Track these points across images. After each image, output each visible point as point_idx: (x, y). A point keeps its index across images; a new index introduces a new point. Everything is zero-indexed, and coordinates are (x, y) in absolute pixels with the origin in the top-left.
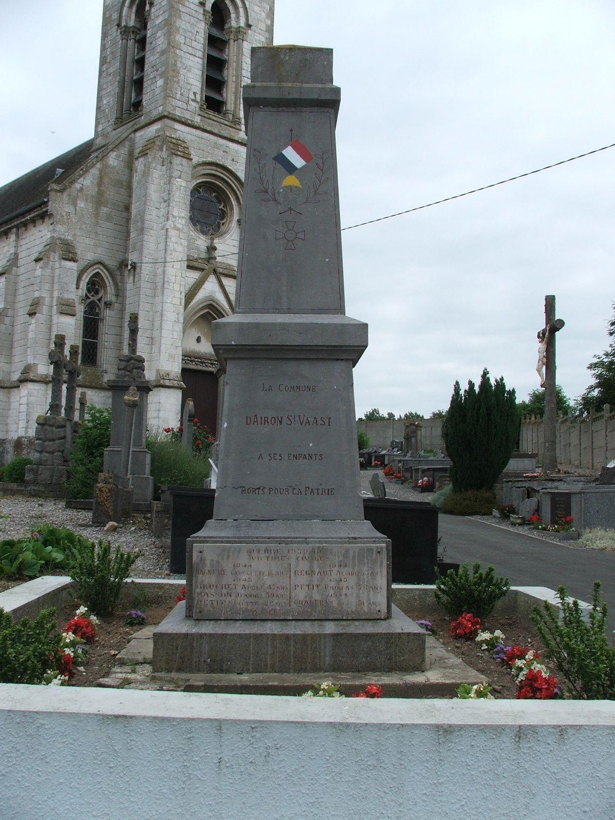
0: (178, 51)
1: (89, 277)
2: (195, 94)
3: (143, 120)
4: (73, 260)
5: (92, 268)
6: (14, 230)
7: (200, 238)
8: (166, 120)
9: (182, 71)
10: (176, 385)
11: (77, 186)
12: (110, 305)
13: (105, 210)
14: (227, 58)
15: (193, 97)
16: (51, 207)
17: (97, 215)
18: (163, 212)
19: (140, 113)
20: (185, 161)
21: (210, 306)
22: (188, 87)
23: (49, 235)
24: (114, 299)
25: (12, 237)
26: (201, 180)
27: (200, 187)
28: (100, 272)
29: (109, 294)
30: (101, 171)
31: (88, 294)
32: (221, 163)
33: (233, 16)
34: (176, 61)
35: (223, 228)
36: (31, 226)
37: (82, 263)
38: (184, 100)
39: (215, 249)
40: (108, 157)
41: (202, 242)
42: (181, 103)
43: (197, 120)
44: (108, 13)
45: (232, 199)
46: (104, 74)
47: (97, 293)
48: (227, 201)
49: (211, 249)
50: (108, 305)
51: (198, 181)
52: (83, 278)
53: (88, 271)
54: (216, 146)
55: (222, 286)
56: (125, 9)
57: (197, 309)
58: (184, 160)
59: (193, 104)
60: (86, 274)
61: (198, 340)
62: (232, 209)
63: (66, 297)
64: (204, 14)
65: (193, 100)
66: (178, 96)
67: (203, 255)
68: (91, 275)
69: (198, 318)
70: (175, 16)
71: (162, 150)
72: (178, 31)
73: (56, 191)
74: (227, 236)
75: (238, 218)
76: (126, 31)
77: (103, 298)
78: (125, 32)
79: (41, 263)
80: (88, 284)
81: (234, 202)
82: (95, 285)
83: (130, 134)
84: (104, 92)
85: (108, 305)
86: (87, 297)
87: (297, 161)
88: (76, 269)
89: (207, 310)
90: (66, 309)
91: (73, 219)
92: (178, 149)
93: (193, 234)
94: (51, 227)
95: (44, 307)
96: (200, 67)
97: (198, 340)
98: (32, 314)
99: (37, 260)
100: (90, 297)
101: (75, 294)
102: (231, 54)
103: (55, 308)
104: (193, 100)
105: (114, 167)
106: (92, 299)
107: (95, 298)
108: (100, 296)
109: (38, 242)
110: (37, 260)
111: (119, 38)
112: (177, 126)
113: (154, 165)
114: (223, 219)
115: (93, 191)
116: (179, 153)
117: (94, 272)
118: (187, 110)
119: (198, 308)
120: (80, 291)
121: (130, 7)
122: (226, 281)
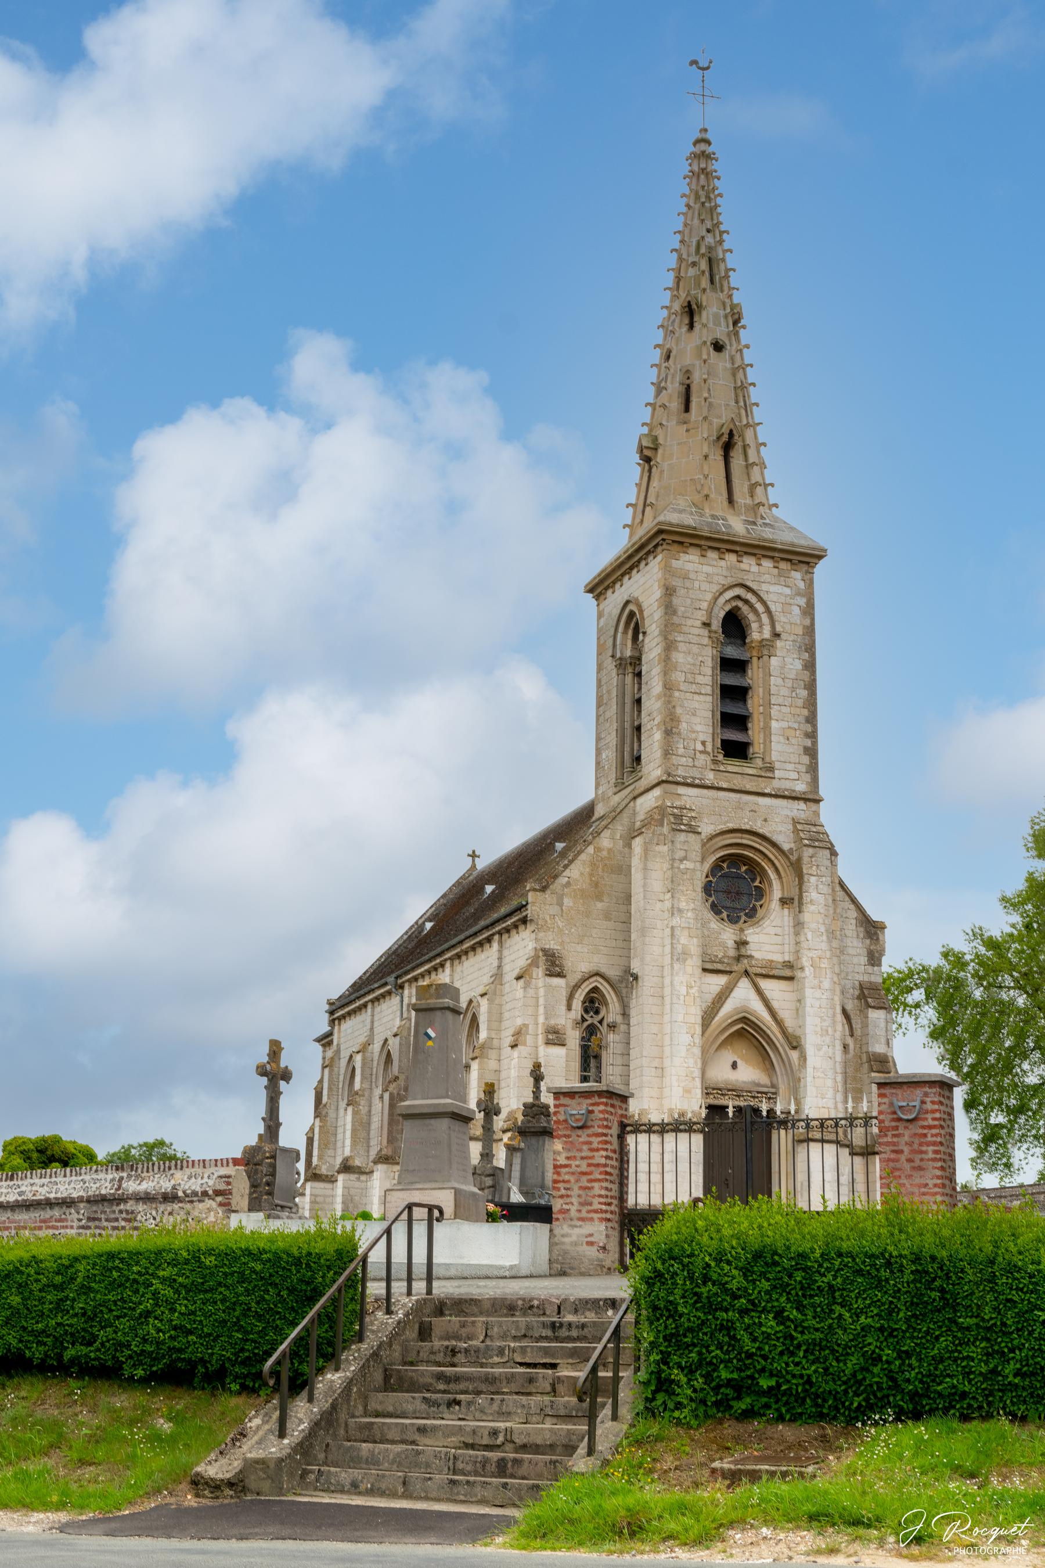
0: (677, 694)
1: (584, 993)
2: (703, 743)
3: (643, 784)
4: (560, 975)
5: (587, 982)
6: (496, 937)
8: (664, 785)
9: (684, 718)
11: (562, 880)
14: (750, 682)
16: (530, 912)
18: (668, 904)
19: (640, 774)
20: (692, 837)
21: (744, 1020)
22: (694, 736)
23: (531, 945)
24: (619, 1019)
25: (495, 945)
27: (723, 862)
29: (612, 1012)
32: (747, 827)
33: (754, 626)
35: (760, 912)
36: (514, 932)
37: (574, 978)
39: (745, 943)
41: (728, 935)
43: (710, 777)
44: (602, 638)
45: (769, 872)
46: (601, 719)
47: (597, 1012)
48: (763, 873)
49: (741, 944)
50: (612, 1027)
52: (577, 996)
53: (583, 987)
54: (739, 807)
56: (619, 635)
57: (724, 1025)
58: (691, 834)
59: (703, 757)
60: (580, 990)
61: (734, 1066)
62: (770, 885)
64: (710, 637)
65: (701, 752)
66: (681, 751)
67: (732, 953)
68: (587, 990)
69: (731, 1035)
71: (662, 825)
72: (675, 668)
73: (535, 890)
74: (766, 923)
75: (780, 896)
76: (621, 664)
78: (620, 664)
79: (521, 982)
80: (584, 1002)
81: (772, 875)
82: (593, 1003)
84: (602, 743)
85: (612, 1027)
86: (584, 1020)
87: (432, 1034)
88: (564, 986)
90: (555, 1037)
92: (681, 822)
93: (714, 924)
94: (533, 936)
96: (709, 706)
97: (734, 1066)
98: (514, 1046)
99: (518, 978)
101: (567, 1019)
102: (755, 678)
103: (540, 1037)
104: (701, 752)
107: (595, 1020)
108: (600, 1016)
109: (521, 953)
110: (518, 978)
111: (614, 673)
112: (681, 790)
114: (760, 899)
116: (683, 827)
117: (591, 987)
118: (694, 766)
119: (726, 1023)
121: (625, 632)
122: (765, 984)
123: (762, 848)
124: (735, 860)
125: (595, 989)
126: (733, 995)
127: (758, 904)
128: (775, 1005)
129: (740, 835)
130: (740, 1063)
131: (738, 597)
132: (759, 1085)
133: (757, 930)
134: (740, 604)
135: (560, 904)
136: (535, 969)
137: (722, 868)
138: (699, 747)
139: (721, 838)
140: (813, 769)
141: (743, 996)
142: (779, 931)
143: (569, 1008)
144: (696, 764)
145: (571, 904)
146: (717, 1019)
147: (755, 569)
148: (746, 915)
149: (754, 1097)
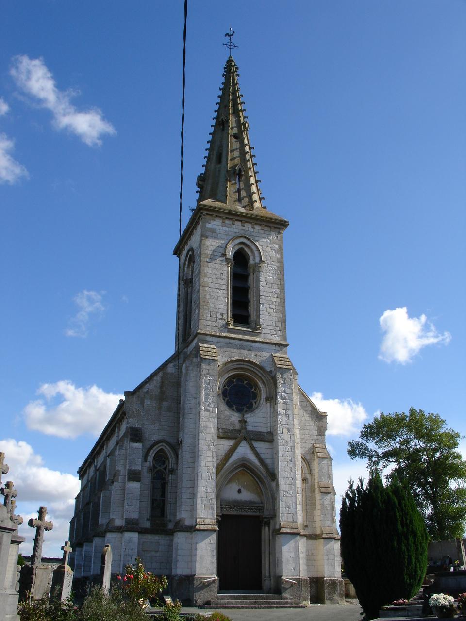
1: (155, 452)
2: (222, 314)
7: (234, 415)
10: (211, 529)
12: (172, 471)
13: (165, 404)
15: (220, 317)
17: (160, 408)
26: (233, 373)
28: (164, 448)
30: (162, 378)
31: (156, 465)
33: (251, 258)
34: (205, 295)
37: (148, 444)
38: (213, 320)
40: (167, 368)
41: (235, 417)
42: (211, 322)
45: (259, 383)
49: (243, 422)
51: (230, 375)
52: (150, 454)
55: (253, 449)
60: (152, 451)
61: (239, 491)
63: (134, 468)
65: (220, 319)
66: (209, 318)
70: (204, 266)
74: (257, 411)
77: (168, 467)
82: (161, 457)
83: (184, 349)
86: (155, 467)
89: (242, 468)
91: (142, 413)
95: (120, 477)
97: (239, 491)
100: (157, 467)
104: (220, 319)
105: (172, 374)
106: (159, 468)
107: (162, 468)
113: (191, 368)
114: (255, 399)
115: (157, 392)
117: (159, 448)
120: (148, 463)
122: (257, 445)
123: (255, 370)
124: (239, 378)
125: (161, 450)
126: (237, 451)
127: (254, 402)
128: (263, 456)
129: (250, 372)
130: (242, 490)
131: (242, 243)
132: (254, 502)
133: (252, 415)
134: (244, 247)
135: (142, 403)
136: (125, 438)
137: (233, 382)
138: (220, 316)
139: (231, 364)
140: (283, 329)
141: (244, 450)
142: (265, 415)
143: (146, 461)
144: (217, 325)
145: (149, 403)
146: (227, 464)
147: (251, 229)
148: (247, 407)
149: (250, 509)
